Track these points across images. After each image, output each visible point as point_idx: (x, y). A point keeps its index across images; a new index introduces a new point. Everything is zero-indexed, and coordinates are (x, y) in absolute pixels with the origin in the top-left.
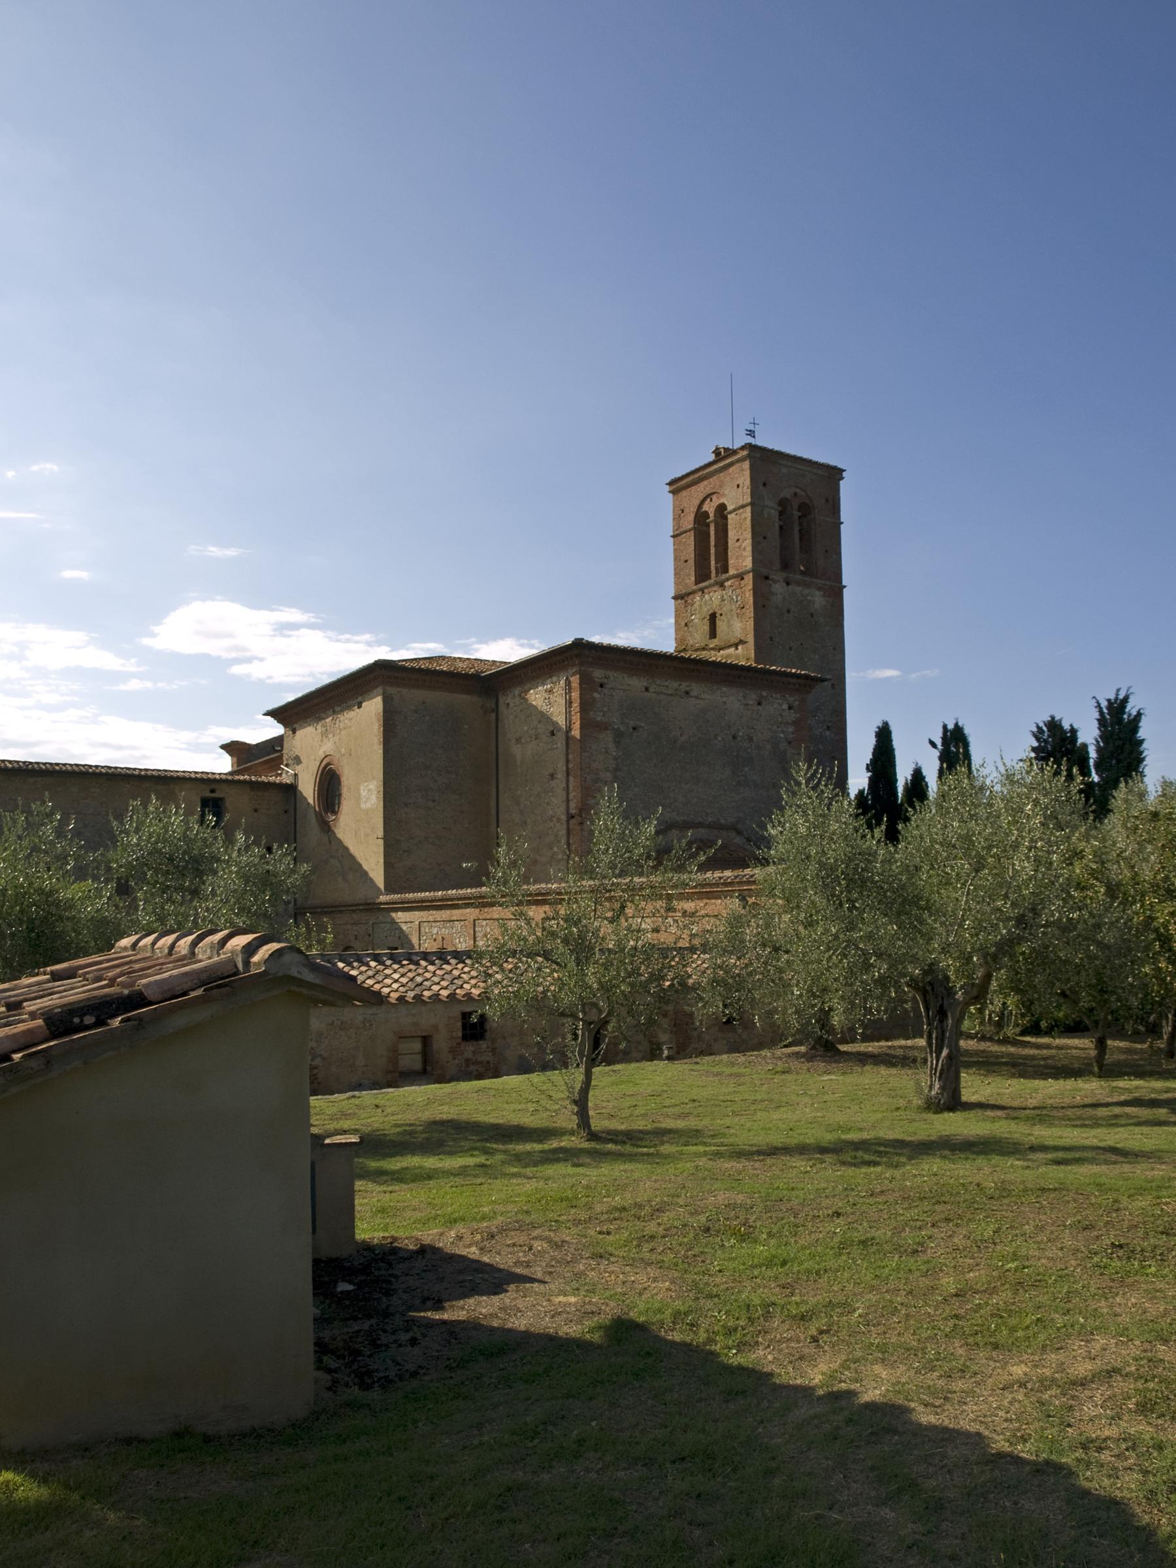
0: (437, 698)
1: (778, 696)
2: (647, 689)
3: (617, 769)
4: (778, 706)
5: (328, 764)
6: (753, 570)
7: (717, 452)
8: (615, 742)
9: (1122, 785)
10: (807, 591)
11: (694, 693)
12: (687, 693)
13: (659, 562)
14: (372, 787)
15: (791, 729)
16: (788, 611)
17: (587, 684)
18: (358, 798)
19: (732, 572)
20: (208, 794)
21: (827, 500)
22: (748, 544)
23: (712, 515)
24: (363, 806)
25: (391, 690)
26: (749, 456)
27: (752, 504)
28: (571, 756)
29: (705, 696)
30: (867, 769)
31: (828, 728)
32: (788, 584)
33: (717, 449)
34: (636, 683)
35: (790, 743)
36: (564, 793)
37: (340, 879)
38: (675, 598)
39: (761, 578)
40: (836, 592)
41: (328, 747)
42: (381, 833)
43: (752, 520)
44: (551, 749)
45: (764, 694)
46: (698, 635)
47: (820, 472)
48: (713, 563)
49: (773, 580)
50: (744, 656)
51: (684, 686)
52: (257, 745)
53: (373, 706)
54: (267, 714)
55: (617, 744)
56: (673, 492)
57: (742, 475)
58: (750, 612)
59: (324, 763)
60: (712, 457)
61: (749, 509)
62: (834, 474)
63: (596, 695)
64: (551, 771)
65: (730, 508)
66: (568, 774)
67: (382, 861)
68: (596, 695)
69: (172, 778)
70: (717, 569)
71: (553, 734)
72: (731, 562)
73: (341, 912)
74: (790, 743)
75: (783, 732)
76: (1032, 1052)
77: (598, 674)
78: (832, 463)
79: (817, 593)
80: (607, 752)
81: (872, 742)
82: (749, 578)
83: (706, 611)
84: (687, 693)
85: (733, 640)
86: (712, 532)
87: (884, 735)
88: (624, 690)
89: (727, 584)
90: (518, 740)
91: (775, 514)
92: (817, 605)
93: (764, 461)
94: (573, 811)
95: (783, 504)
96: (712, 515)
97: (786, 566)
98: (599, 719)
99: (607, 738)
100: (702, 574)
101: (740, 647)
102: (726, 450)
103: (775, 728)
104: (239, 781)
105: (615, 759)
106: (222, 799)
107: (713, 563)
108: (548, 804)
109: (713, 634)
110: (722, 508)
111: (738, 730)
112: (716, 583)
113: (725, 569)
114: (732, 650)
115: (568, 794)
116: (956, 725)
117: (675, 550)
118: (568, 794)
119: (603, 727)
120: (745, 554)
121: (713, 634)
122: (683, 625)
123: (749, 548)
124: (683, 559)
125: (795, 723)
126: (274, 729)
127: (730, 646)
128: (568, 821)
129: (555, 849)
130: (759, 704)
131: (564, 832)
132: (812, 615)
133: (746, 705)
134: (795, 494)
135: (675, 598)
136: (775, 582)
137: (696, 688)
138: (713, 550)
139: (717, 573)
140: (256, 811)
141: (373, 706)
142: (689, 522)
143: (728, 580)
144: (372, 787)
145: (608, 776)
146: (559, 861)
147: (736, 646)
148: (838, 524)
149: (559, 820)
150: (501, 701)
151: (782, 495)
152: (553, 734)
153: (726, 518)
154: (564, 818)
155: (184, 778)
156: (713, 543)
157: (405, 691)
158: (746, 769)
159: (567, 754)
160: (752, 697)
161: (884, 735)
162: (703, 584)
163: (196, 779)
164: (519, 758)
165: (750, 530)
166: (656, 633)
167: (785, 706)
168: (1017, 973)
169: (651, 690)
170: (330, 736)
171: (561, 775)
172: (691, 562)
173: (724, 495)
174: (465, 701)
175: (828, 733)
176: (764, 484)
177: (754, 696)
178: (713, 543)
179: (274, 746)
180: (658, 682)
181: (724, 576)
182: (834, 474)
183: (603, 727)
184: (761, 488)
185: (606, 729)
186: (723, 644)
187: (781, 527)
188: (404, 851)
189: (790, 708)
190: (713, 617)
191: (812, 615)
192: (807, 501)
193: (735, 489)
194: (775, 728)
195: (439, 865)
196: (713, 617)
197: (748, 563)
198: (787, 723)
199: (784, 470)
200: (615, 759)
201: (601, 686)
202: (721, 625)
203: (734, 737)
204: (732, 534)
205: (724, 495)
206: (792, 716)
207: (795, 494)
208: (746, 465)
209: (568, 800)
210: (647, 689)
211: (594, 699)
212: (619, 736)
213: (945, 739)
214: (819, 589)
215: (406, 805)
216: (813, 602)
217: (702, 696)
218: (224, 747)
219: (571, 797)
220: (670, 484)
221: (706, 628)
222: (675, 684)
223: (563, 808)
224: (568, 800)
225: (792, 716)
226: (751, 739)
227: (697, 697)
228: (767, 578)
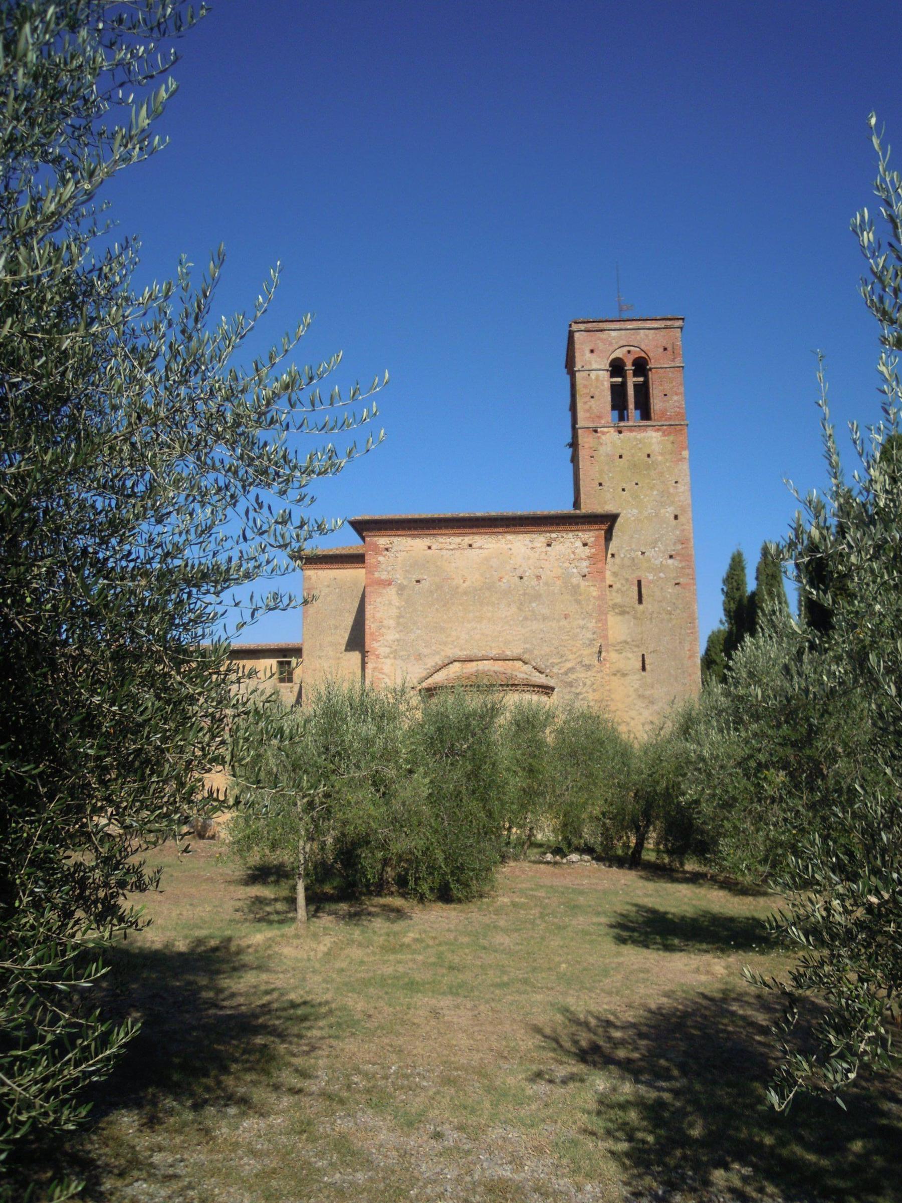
3: (399, 617)
9: (748, 638)
12: (470, 546)
16: (621, 457)
32: (620, 432)
45: (554, 535)
51: (467, 540)
63: (381, 558)
75: (576, 567)
76: (229, 1012)
80: (390, 604)
84: (470, 546)
105: (399, 608)
111: (525, 571)
130: (549, 545)
134: (629, 352)
145: (392, 623)
151: (613, 356)
157: (320, 572)
158: (534, 605)
167: (579, 544)
168: (458, 881)
176: (592, 351)
185: (390, 584)
192: (643, 355)
200: (399, 608)
201: (387, 549)
210: (429, 548)
212: (401, 588)
217: (486, 546)
222: (458, 540)
226: (539, 577)
227: (480, 548)
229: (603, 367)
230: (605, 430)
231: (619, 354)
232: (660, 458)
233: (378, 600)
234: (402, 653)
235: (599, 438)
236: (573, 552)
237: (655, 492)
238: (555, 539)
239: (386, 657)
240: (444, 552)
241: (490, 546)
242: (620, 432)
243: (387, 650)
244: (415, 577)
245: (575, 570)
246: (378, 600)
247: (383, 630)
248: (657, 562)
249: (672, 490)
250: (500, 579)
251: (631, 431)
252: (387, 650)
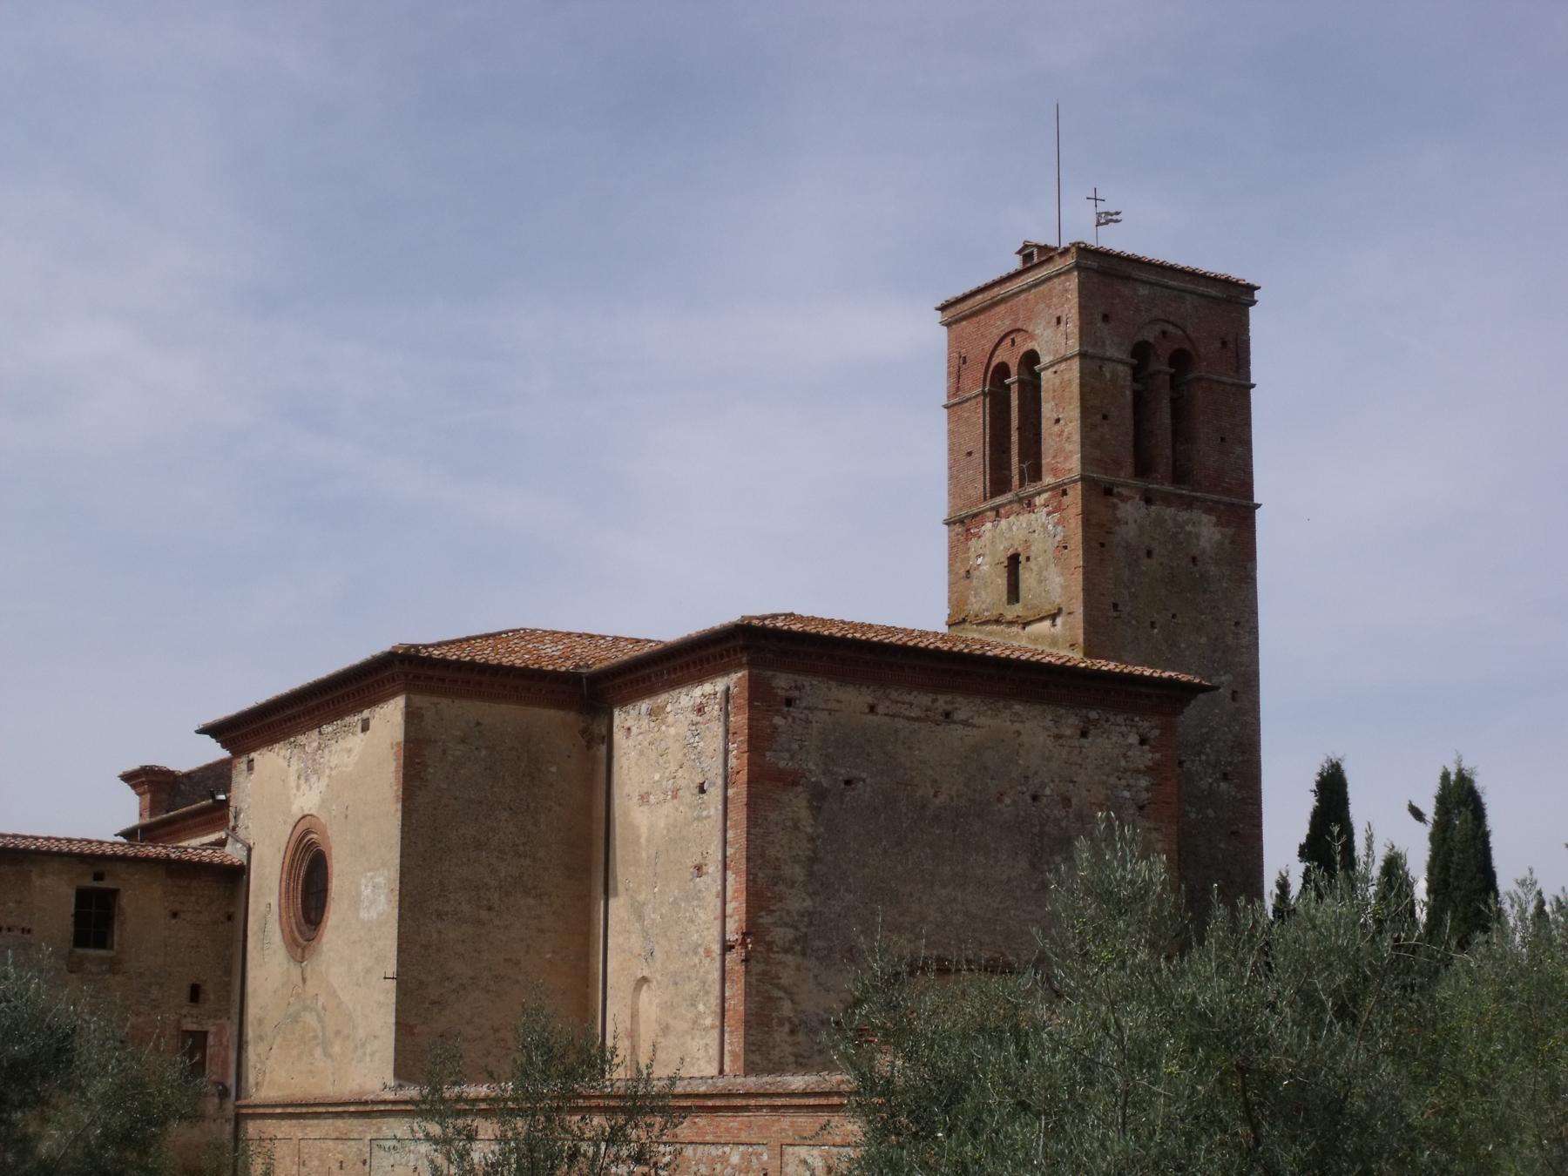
0: (504, 716)
1: (1120, 719)
2: (872, 709)
3: (814, 859)
4: (1120, 741)
5: (308, 832)
6: (1083, 479)
7: (1026, 252)
8: (811, 807)
10: (1184, 515)
11: (961, 715)
12: (947, 715)
13: (920, 447)
14: (380, 880)
15: (1144, 783)
16: (1149, 554)
17: (760, 697)
18: (356, 900)
19: (1048, 479)
20: (89, 882)
21: (1224, 344)
22: (1073, 427)
23: (1014, 369)
24: (364, 915)
25: (420, 701)
26: (1078, 267)
27: (1082, 355)
28: (730, 834)
29: (984, 721)
30: (1301, 854)
31: (1225, 777)
32: (1148, 501)
33: (1026, 247)
34: (853, 698)
35: (1141, 808)
36: (719, 903)
37: (318, 1052)
38: (949, 523)
39: (1098, 491)
40: (1239, 514)
41: (307, 800)
42: (391, 968)
43: (1082, 385)
44: (698, 818)
45: (1093, 715)
46: (989, 593)
47: (1212, 292)
48: (1015, 460)
49: (1120, 495)
50: (1056, 640)
51: (942, 702)
52: (189, 776)
53: (389, 717)
54: (205, 730)
55: (816, 810)
56: (948, 325)
57: (1067, 295)
58: (1076, 557)
59: (300, 828)
60: (1016, 263)
61: (1075, 364)
62: (1233, 298)
63: (778, 720)
64: (699, 860)
65: (1045, 359)
66: (725, 867)
67: (392, 1020)
68: (778, 720)
69: (26, 853)
70: (1021, 473)
71: (702, 790)
72: (1046, 460)
73: (317, 1115)
74: (1141, 808)
75: (1128, 787)
77: (782, 682)
78: (1236, 274)
79: (1205, 518)
80: (796, 828)
81: (1310, 802)
82: (1075, 496)
83: (1002, 552)
84: (947, 715)
85: (1049, 608)
86: (1015, 403)
87: (1332, 791)
88: (830, 712)
89: (1039, 500)
90: (644, 798)
91: (1124, 372)
92: (1204, 543)
93: (1105, 273)
94: (732, 937)
95: (1141, 352)
96: (1014, 369)
97: (1143, 467)
98: (782, 764)
99: (797, 804)
100: (999, 484)
101: (1059, 621)
102: (1043, 249)
103: (1112, 780)
104: (147, 860)
105: (811, 839)
106: (114, 893)
107: (1015, 460)
108: (691, 921)
109: (1014, 593)
110: (1031, 358)
111: (1043, 786)
112: (1020, 500)
113: (1035, 473)
114: (1047, 623)
115: (724, 903)
116: (1460, 773)
117: (951, 432)
118: (724, 903)
119: (790, 780)
120: (1069, 447)
121: (1014, 593)
122: (961, 575)
123: (1077, 437)
124: (965, 449)
125: (1149, 770)
126: (214, 752)
127: (1042, 619)
128: (723, 955)
129: (701, 1007)
130: (1084, 734)
131: (716, 975)
132: (1194, 559)
133: (1058, 737)
134: (1164, 333)
135: (949, 523)
136: (1124, 499)
137: (964, 708)
138: (1015, 437)
139: (1021, 485)
140: (175, 915)
141: (389, 717)
142: (974, 386)
143: (1039, 494)
144: (380, 880)
145: (798, 872)
146: (706, 1029)
147: (1053, 617)
148: (1246, 388)
149: (708, 953)
150: (617, 722)
151: (1139, 338)
152: (702, 790)
153: (1038, 376)
154: (716, 948)
155: (49, 854)
156: (1015, 423)
157: (444, 702)
159: (725, 831)
160: (1071, 723)
161: (1332, 791)
162: (999, 500)
163: (70, 854)
164: (644, 831)
165: (1076, 403)
166: (905, 595)
167: (1133, 739)
169: (881, 709)
170: (313, 779)
171: (713, 869)
172: (977, 456)
173: (1032, 337)
174: (549, 720)
175: (1223, 786)
177: (1073, 720)
178: (1015, 423)
179: (216, 778)
180: (894, 695)
181: (1030, 489)
182: (1233, 298)
183: (790, 780)
184: (1100, 324)
185: (795, 783)
186: (1030, 615)
187: (1137, 395)
188: (433, 1003)
189: (1143, 742)
190: (1014, 562)
191: (1194, 559)
192: (1187, 346)
193: (1055, 334)
194: (1112, 780)
195: (496, 1031)
196: (1014, 562)
197: (1074, 465)
198: (1138, 771)
199: (1143, 291)
200: (811, 839)
202: (1027, 578)
203: (1035, 798)
204: (1048, 410)
205: (1032, 337)
206: (1144, 757)
207: (1164, 333)
208: (1073, 282)
209: (724, 916)
210: (872, 709)
211: (776, 728)
212: (818, 796)
213: (1442, 800)
214: (1209, 511)
215: (439, 916)
216: (1198, 536)
217: (976, 721)
218: (128, 778)
219: (729, 911)
220: (943, 308)
221: (1002, 582)
222: (926, 700)
223: (715, 931)
224: (724, 916)
225: (1144, 757)
226: (1066, 801)
227: (965, 723)
228: (1108, 492)
229: (1125, 357)
230: (1125, 492)
231: (1149, 335)
232: (1212, 569)
233: (773, 817)
234: (818, 943)
235: (1115, 507)
236: (1125, 756)
237: (1203, 640)
238: (1096, 723)
239: (786, 951)
240: (900, 723)
241: (983, 721)
242: (1148, 501)
243: (790, 934)
244: (843, 773)
245: (1127, 794)
246: (773, 817)
247: (782, 887)
248: (1204, 784)
249: (1230, 639)
250: (1000, 797)
251: (1169, 504)
252: (790, 934)
